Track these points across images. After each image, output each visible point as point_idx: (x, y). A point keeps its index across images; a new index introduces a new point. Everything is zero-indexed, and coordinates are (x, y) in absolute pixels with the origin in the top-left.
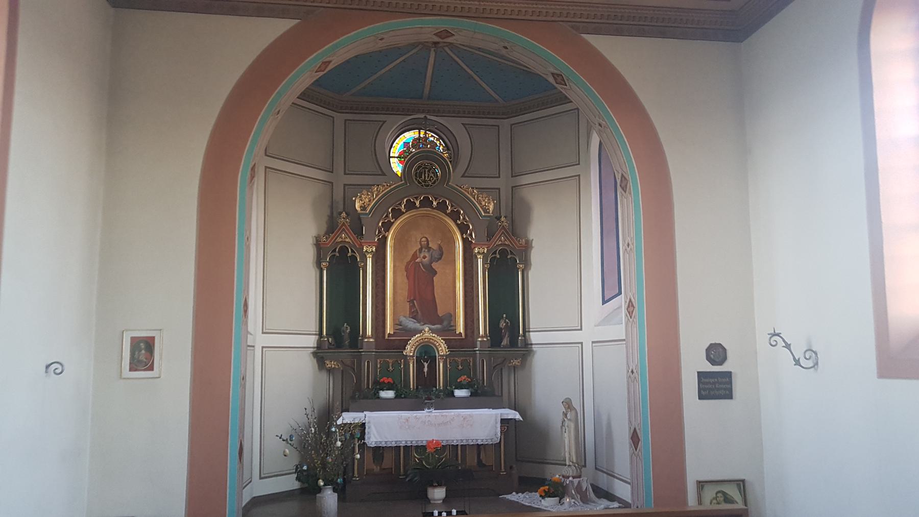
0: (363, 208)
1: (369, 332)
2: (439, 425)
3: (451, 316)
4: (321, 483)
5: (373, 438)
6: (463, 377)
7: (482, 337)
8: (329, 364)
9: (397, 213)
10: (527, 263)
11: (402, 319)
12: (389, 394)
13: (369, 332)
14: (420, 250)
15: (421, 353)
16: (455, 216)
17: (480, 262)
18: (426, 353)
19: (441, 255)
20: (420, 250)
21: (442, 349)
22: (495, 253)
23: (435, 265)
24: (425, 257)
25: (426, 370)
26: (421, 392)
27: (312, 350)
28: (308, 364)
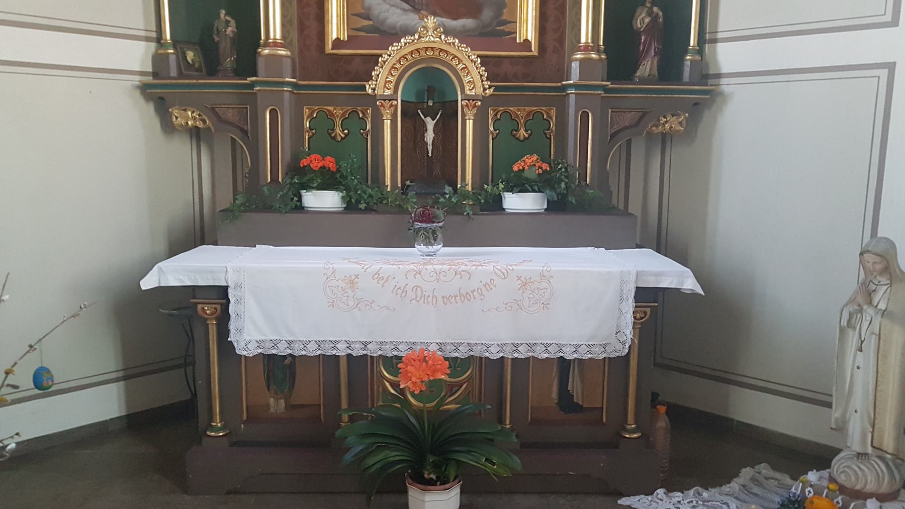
1: (276, 30)
2: (446, 299)
5: (251, 332)
6: (530, 159)
7: (586, 48)
8: (188, 117)
12: (323, 200)
13: (276, 30)
15: (419, 94)
18: (431, 91)
21: (473, 81)
25: (430, 136)
27: (137, 79)
28: (127, 121)
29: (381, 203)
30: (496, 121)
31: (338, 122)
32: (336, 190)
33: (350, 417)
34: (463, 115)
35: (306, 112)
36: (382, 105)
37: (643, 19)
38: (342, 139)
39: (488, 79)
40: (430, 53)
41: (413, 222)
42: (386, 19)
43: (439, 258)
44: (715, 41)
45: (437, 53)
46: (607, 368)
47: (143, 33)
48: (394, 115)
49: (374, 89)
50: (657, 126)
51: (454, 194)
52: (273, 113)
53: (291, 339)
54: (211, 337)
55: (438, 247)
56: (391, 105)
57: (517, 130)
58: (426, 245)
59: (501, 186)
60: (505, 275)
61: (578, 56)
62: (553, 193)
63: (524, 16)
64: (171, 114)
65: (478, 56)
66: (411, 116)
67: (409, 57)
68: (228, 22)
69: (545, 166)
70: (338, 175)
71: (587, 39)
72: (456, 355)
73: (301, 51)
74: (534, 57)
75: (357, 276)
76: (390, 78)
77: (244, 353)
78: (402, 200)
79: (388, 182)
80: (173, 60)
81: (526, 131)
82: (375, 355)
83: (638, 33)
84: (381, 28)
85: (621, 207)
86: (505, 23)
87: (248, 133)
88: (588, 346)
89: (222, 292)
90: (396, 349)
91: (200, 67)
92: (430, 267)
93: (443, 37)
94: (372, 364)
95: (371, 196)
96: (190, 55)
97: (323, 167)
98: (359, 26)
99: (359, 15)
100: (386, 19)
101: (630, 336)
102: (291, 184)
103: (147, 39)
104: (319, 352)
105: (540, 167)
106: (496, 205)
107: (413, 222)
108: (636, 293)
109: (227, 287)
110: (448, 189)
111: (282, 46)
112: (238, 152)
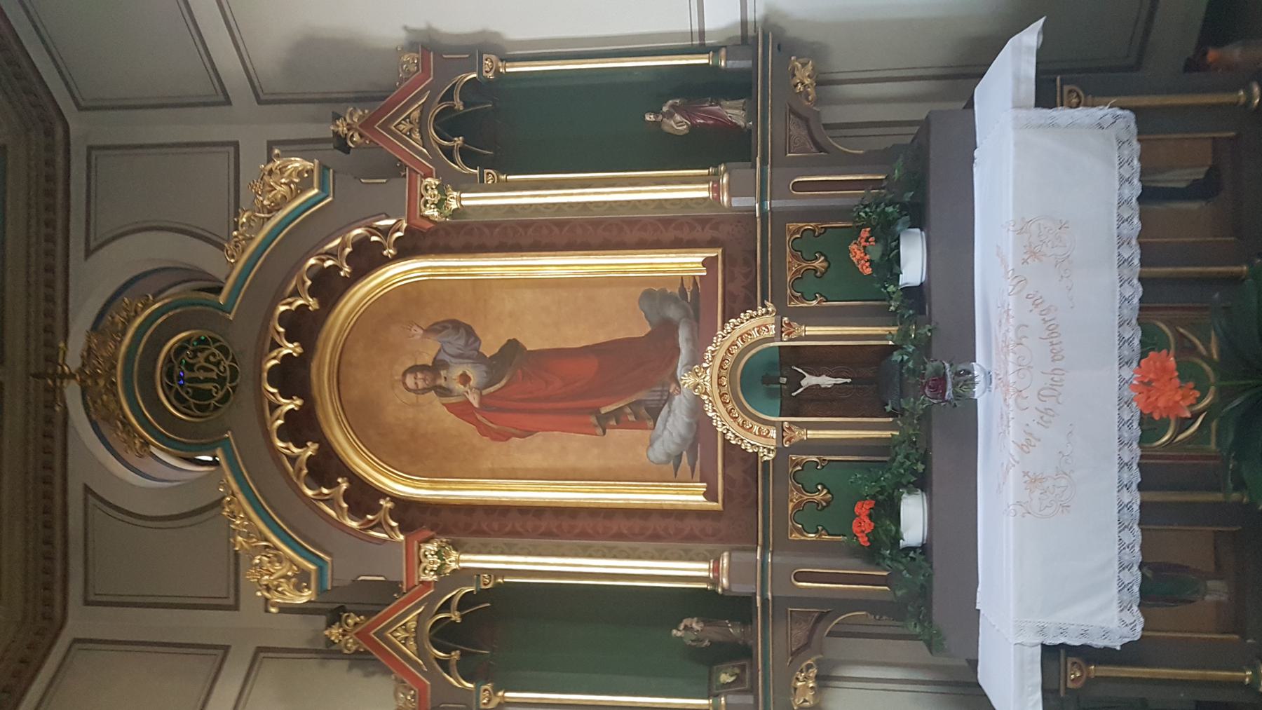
0: (302, 578)
3: (648, 295)
4: (650, 117)
5: (1110, 619)
7: (716, 190)
9: (326, 467)
10: (480, 47)
11: (659, 451)
12: (914, 519)
13: (700, 569)
14: (444, 392)
15: (771, 394)
16: (329, 287)
17: (473, 199)
18: (768, 380)
19: (456, 325)
20: (444, 392)
21: (757, 327)
22: (448, 152)
23: (490, 345)
24: (465, 379)
25: (826, 381)
30: (804, 298)
32: (900, 500)
33: (1236, 489)
34: (800, 338)
35: (795, 536)
36: (789, 440)
37: (677, 123)
38: (829, 492)
40: (725, 381)
41: (944, 401)
43: (994, 366)
44: (702, 33)
48: (802, 426)
49: (769, 450)
52: (800, 577)
54: (1114, 674)
55: (978, 368)
56: (789, 429)
57: (816, 270)
58: (974, 384)
59: (891, 288)
60: (1021, 280)
61: (726, 199)
62: (900, 221)
63: (675, 267)
65: (725, 321)
66: (793, 406)
67: (730, 406)
68: (686, 628)
69: (865, 233)
71: (703, 190)
72: (1136, 342)
73: (721, 540)
74: (724, 254)
75: (1026, 474)
76: (756, 429)
77: (1139, 628)
79: (887, 434)
81: (816, 259)
82: (1139, 452)
83: (693, 128)
84: (690, 442)
86: (683, 291)
89: (1052, 654)
90: (1129, 423)
91: (739, 667)
92: (1011, 378)
93: (705, 365)
95: (907, 457)
96: (725, 678)
97: (870, 516)
98: (689, 468)
99: (676, 467)
100: (680, 436)
101: (1106, 110)
102: (892, 560)
104: (1136, 527)
105: (867, 240)
106: (917, 295)
107: (944, 401)
108: (1044, 107)
109: (1043, 645)
110: (897, 357)
111: (717, 561)
112: (847, 629)
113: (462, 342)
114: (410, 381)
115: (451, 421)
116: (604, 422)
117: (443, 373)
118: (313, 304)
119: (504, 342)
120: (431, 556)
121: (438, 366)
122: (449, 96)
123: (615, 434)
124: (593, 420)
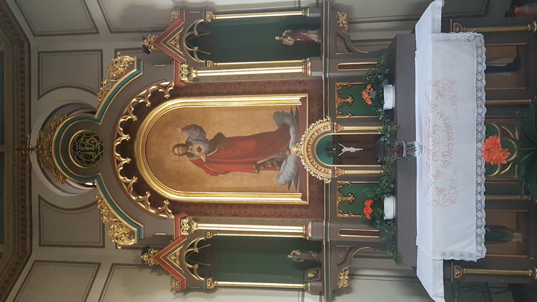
0: (131, 235)
1: (299, 229)
2: (450, 138)
5: (472, 248)
7: (306, 69)
8: (344, 278)
9: (141, 187)
12: (389, 207)
13: (299, 229)
14: (190, 155)
15: (329, 155)
16: (142, 111)
17: (202, 73)
18: (327, 149)
19: (196, 127)
20: (190, 155)
21: (323, 127)
22: (192, 53)
23: (210, 136)
24: (199, 150)
25: (352, 150)
26: (387, 159)
29: (390, 176)
30: (343, 114)
31: (345, 199)
32: (384, 200)
33: (525, 194)
34: (341, 132)
35: (340, 215)
36: (337, 174)
38: (354, 197)
39: (322, 119)
40: (309, 150)
42: (291, 173)
43: (424, 143)
45: (309, 146)
46: (491, 45)
47: (300, 298)
49: (328, 179)
50: (344, 28)
51: (385, 135)
52: (342, 232)
53: (475, 226)
55: (417, 144)
56: (337, 170)
57: (348, 103)
58: (415, 150)
59: (380, 110)
60: (435, 106)
61: (310, 72)
62: (384, 82)
63: (288, 102)
64: (342, 287)
65: (309, 124)
66: (340, 159)
67: (312, 160)
69: (369, 87)
70: (375, 199)
72: (484, 132)
73: (308, 217)
76: (323, 170)
77: (484, 253)
78: (389, 164)
79: (378, 172)
80: (314, 284)
81: (348, 98)
82: (485, 179)
83: (296, 42)
85: (390, 43)
87: (353, 246)
88: (477, 57)
89: (448, 264)
92: (431, 148)
93: (301, 143)
94: (490, 181)
95: (387, 181)
96: (310, 275)
97: (371, 207)
100: (291, 173)
101: (471, 33)
102: (380, 225)
103: (303, 296)
106: (391, 113)
108: (445, 32)
109: (444, 261)
110: (382, 139)
111: (307, 226)
112: (362, 254)
113: (198, 134)
114: (176, 151)
115: (194, 167)
116: (258, 168)
117: (190, 147)
118: (135, 118)
119: (216, 134)
120: (186, 224)
121: (187, 144)
122: (191, 29)
123: (263, 173)
124: (254, 166)
